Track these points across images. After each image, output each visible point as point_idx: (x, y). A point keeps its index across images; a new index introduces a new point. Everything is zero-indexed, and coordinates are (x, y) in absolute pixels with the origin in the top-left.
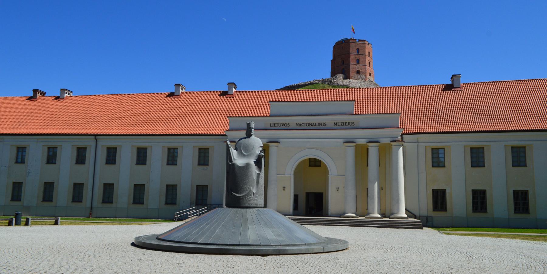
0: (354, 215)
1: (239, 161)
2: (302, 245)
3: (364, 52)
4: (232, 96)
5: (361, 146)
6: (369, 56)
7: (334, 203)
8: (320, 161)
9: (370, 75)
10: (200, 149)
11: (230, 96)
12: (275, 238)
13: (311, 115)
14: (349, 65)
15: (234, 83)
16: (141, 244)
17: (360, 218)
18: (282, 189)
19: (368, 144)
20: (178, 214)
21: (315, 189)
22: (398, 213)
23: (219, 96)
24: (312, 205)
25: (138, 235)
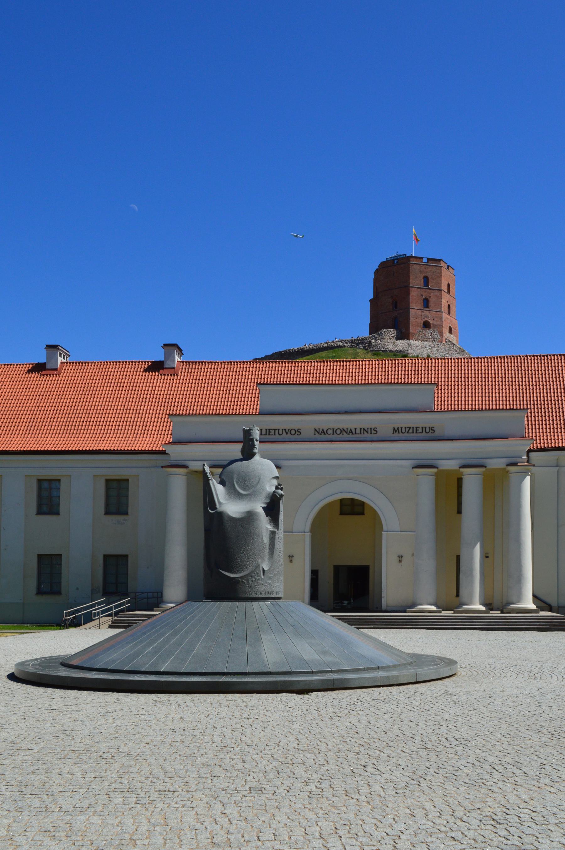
0: (434, 608)
1: (232, 508)
2: (372, 669)
3: (440, 284)
4: (173, 372)
5: (448, 473)
6: (449, 292)
7: (392, 583)
8: (362, 504)
9: (450, 331)
10: (108, 481)
11: (171, 371)
12: (317, 657)
13: (346, 412)
14: (407, 310)
15: (176, 345)
16: (31, 677)
17: (445, 613)
18: (397, 559)
19: (462, 470)
20: (70, 614)
21: (353, 558)
22: (518, 602)
23: (145, 371)
24: (348, 589)
25: (20, 660)
